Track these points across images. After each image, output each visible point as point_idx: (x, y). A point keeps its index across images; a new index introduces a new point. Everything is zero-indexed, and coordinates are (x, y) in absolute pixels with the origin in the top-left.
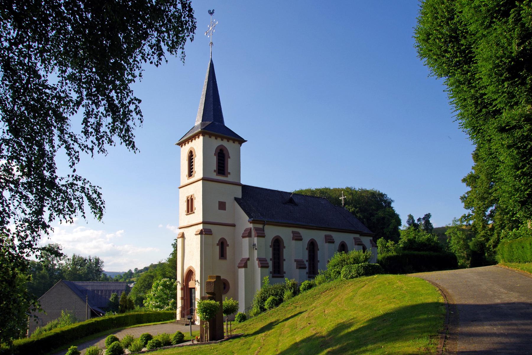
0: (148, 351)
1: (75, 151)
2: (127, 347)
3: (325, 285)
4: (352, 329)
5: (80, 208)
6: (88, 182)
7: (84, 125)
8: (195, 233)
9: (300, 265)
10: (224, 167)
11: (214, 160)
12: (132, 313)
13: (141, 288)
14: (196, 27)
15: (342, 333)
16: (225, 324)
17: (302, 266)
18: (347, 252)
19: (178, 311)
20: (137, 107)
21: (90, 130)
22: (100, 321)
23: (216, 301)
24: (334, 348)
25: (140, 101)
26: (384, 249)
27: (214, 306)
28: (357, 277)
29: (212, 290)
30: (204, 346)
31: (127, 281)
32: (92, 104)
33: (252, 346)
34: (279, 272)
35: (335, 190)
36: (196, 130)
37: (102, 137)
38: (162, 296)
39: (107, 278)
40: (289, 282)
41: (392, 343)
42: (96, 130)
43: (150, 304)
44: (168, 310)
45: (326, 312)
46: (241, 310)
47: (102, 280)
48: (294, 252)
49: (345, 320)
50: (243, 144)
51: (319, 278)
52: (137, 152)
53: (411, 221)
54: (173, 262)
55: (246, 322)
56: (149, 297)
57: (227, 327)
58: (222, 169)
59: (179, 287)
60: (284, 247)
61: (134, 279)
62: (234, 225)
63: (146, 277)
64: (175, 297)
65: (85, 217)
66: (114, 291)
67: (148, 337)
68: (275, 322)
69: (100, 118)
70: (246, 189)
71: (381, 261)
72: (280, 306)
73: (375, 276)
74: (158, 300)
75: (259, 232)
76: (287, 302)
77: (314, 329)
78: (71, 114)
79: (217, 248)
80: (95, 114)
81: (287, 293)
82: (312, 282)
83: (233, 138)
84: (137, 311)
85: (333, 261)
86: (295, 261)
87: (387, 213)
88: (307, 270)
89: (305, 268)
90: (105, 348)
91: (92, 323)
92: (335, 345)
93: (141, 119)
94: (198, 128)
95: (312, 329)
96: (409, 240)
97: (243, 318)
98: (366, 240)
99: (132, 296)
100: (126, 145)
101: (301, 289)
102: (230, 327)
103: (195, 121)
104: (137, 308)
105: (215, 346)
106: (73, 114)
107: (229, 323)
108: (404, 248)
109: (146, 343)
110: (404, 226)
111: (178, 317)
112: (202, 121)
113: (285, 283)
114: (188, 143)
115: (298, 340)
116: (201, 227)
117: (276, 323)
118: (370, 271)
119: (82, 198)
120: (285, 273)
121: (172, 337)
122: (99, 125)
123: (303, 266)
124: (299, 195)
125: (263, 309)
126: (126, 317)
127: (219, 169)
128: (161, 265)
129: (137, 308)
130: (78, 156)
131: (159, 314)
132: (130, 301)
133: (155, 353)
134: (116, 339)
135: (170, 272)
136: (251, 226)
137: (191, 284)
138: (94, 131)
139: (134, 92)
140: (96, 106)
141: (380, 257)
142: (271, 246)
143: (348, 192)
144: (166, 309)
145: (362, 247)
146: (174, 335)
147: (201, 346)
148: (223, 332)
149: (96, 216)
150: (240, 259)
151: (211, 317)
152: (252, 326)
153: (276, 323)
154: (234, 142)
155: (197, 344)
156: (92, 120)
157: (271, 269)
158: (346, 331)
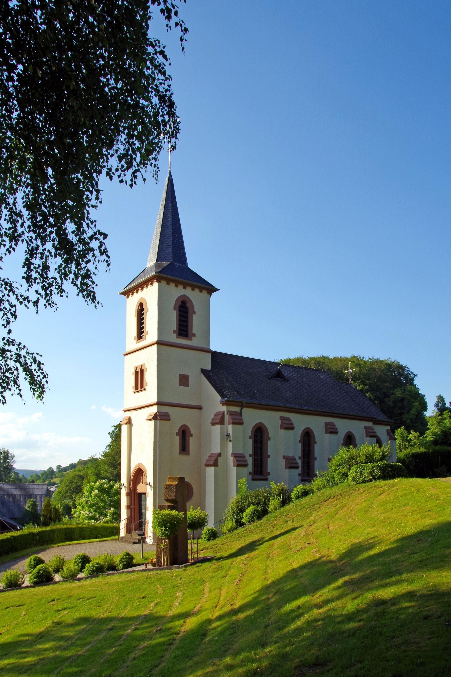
0: (87, 578)
1: (10, 305)
2: (57, 571)
3: (327, 492)
4: (375, 551)
5: (15, 383)
6: (24, 347)
7: (26, 269)
8: (146, 418)
9: (290, 464)
10: (186, 326)
11: (173, 316)
12: (59, 526)
13: (67, 492)
14: (179, 130)
15: (361, 558)
16: (190, 541)
17: (292, 465)
18: (355, 446)
19: (123, 524)
20: (101, 244)
21: (34, 275)
22: (18, 537)
23: (179, 512)
24: (353, 576)
25: (105, 236)
26: (403, 444)
27: (176, 518)
28: (370, 481)
29: (172, 496)
30: (162, 572)
31: (47, 482)
32: (36, 238)
33: (230, 573)
34: (261, 473)
35: (336, 359)
36: (149, 274)
37: (50, 285)
38: (97, 504)
39: (19, 479)
40: (275, 487)
41: (436, 571)
42: (42, 276)
43: (82, 515)
44: (105, 522)
45: (331, 528)
46: (210, 525)
47: (12, 481)
48: (282, 445)
49: (361, 539)
50: (214, 294)
51: (318, 482)
52: (99, 306)
53: (440, 405)
54: (113, 457)
55: (217, 541)
56: (79, 504)
57: (192, 546)
58: (184, 329)
59: (124, 492)
60: (269, 439)
61: (57, 480)
62: (200, 408)
63: (73, 477)
64: (117, 505)
65: (21, 396)
66: (30, 496)
67: (85, 560)
68: (259, 541)
69: (46, 259)
70: (216, 356)
71: (404, 459)
72: (264, 519)
73: (397, 480)
74: (92, 510)
75: (235, 417)
76: (273, 515)
77: (317, 552)
78: (7, 253)
79: (177, 440)
80: (41, 253)
81: (274, 502)
82: (307, 486)
83: (200, 285)
84: (66, 524)
85: (336, 460)
86: (284, 457)
87: (407, 393)
88: (299, 471)
89: (297, 468)
90: (26, 573)
91: (7, 538)
92: (354, 573)
93: (107, 261)
94: (151, 271)
95: (314, 551)
96: (443, 432)
97: (213, 535)
98: (382, 431)
99: (56, 503)
100: (84, 297)
101: (293, 496)
102: (196, 546)
103: (146, 262)
104: (66, 519)
105: (177, 571)
106: (10, 252)
107: (195, 541)
108: (435, 442)
109: (83, 567)
110: (431, 412)
111: (123, 533)
112: (157, 260)
113: (271, 488)
114: (137, 292)
115: (296, 565)
116: (154, 409)
117: (261, 542)
118: (389, 473)
119: (17, 369)
120: (269, 474)
121: (117, 560)
122: (46, 268)
123: (294, 465)
124: (287, 365)
125: (240, 524)
126: (52, 531)
127: (180, 329)
128: (93, 460)
129: (66, 519)
130: (15, 312)
131: (96, 528)
132: (56, 510)
133: (95, 580)
134: (40, 561)
135: (106, 471)
136: (224, 408)
137: (140, 488)
138: (38, 276)
139: (97, 223)
140: (42, 242)
141: (402, 454)
142: (250, 438)
143: (353, 362)
144: (102, 522)
145: (375, 440)
146: (120, 557)
147: (159, 572)
148: (187, 554)
149: (34, 394)
150: (209, 455)
151: (171, 532)
152: (226, 546)
153: (261, 542)
154: (201, 292)
155: (153, 570)
156: (37, 261)
157: (250, 468)
158: (366, 554)
